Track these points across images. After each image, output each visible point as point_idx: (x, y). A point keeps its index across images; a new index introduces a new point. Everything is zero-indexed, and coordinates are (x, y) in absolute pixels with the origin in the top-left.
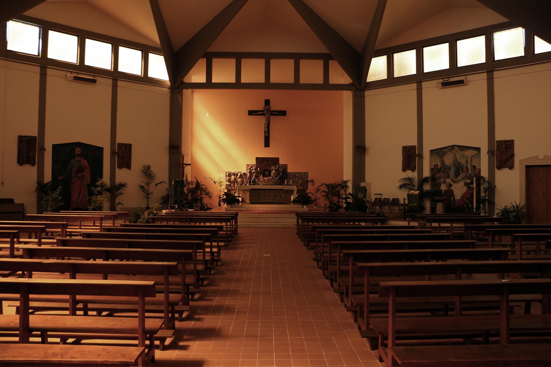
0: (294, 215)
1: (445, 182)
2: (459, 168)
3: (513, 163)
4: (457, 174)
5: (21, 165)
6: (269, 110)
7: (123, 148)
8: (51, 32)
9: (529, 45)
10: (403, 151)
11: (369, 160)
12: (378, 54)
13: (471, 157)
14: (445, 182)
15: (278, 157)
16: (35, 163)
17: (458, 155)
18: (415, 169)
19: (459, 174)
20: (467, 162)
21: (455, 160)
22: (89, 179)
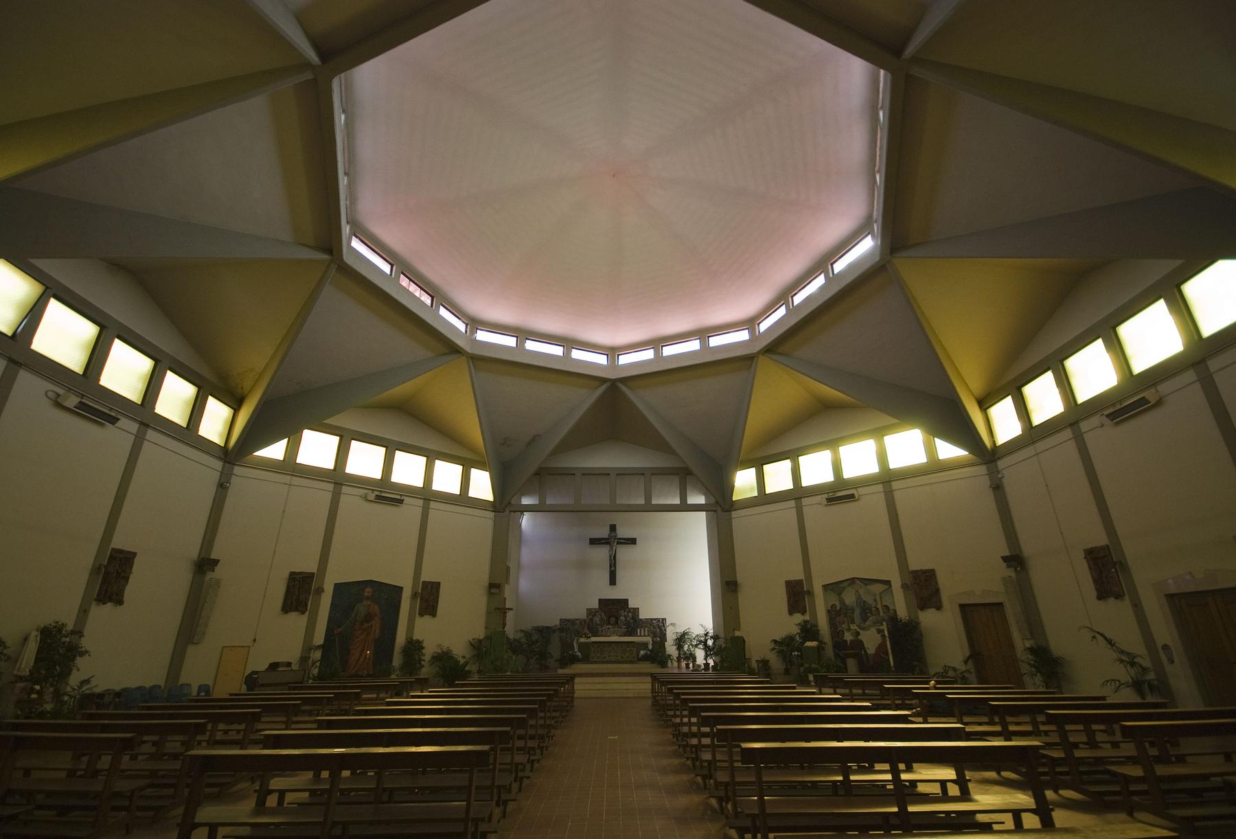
0: (649, 679)
1: (849, 630)
2: (866, 610)
3: (940, 601)
4: (865, 619)
5: (286, 613)
6: (615, 538)
7: (430, 587)
8: (473, 470)
9: (930, 450)
10: (787, 587)
11: (744, 598)
12: (746, 464)
13: (880, 594)
14: (849, 630)
15: (134, 551)
16: (307, 610)
17: (861, 591)
18: (806, 612)
19: (868, 618)
20: (875, 600)
21: (859, 598)
22: (378, 632)
